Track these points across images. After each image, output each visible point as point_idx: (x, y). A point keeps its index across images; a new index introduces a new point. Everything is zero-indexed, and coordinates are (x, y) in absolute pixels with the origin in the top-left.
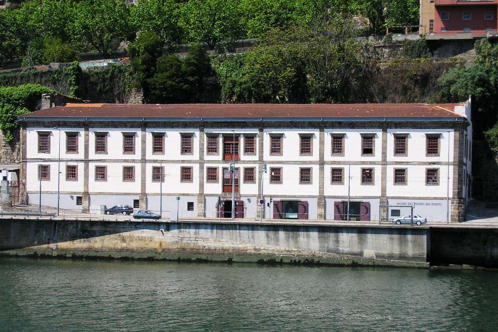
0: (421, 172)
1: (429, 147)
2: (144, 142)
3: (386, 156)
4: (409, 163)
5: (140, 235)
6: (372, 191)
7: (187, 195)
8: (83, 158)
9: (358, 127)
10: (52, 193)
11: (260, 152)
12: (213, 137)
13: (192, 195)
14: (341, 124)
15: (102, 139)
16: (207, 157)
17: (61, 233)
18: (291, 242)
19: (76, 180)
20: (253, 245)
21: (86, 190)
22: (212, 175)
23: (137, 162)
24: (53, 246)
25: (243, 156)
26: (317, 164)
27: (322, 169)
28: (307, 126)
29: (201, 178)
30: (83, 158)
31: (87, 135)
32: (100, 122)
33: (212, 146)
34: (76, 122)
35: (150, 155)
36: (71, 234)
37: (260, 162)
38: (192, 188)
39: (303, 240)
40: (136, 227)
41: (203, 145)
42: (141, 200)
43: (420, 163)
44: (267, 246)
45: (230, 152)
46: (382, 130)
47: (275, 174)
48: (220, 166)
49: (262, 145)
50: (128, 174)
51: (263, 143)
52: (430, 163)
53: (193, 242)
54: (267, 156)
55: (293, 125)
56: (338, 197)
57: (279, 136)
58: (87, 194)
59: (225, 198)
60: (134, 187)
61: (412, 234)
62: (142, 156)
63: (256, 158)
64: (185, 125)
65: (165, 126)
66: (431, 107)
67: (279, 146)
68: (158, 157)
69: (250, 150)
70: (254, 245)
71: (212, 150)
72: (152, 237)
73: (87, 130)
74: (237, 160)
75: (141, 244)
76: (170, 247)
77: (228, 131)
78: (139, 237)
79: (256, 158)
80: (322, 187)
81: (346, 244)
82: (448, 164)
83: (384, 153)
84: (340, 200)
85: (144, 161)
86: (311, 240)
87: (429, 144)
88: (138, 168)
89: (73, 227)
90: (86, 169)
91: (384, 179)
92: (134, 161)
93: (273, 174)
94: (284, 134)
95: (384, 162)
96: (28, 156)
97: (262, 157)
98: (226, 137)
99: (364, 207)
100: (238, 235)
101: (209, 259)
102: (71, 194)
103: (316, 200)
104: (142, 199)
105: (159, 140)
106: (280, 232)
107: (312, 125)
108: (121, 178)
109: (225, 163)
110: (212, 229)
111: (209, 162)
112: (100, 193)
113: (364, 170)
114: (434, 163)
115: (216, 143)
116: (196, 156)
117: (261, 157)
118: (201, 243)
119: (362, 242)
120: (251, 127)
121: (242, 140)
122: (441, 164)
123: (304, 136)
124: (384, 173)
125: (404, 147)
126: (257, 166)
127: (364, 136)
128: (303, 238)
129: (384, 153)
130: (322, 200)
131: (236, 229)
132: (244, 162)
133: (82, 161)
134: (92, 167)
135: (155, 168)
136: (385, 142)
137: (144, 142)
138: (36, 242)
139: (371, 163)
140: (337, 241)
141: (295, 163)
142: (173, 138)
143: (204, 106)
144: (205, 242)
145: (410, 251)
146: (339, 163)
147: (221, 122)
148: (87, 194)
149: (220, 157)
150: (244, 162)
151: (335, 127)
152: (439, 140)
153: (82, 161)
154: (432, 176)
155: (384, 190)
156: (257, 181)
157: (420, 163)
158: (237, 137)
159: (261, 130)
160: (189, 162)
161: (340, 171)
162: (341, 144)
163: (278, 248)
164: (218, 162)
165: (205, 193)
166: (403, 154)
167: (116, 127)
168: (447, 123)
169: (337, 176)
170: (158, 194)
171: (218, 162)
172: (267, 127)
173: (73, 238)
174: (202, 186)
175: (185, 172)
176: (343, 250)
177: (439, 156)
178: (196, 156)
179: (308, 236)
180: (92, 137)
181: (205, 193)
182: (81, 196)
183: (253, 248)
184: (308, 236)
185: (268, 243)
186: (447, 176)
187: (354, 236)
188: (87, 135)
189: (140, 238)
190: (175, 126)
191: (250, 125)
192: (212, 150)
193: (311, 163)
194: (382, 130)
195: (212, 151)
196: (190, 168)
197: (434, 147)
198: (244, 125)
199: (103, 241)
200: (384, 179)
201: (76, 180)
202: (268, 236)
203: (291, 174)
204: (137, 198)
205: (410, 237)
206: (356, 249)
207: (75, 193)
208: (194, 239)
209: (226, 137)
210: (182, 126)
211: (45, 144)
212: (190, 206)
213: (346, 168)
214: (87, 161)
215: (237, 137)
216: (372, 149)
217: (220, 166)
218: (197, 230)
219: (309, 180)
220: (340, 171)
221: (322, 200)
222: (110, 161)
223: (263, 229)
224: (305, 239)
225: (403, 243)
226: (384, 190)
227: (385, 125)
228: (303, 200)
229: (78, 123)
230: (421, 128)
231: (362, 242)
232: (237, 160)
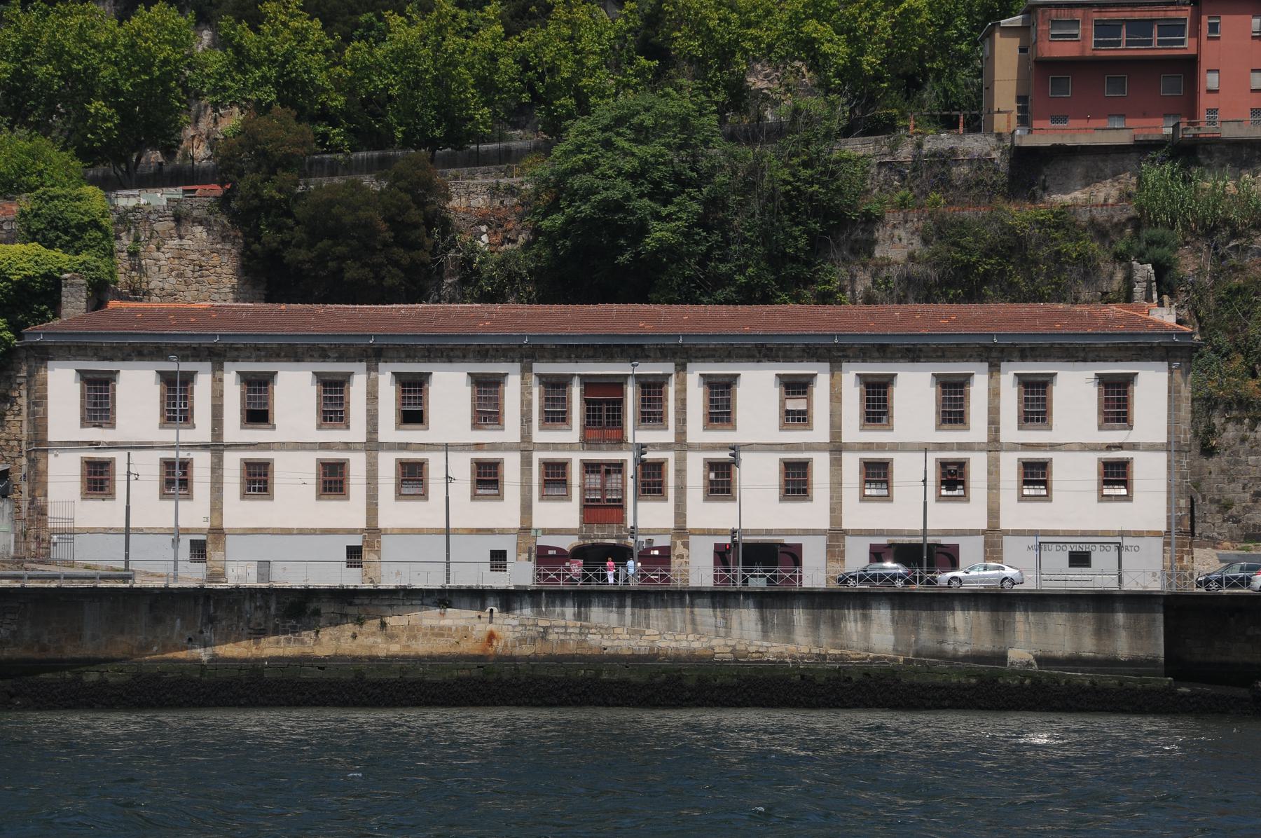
0: (148, 466)
1: (1106, 407)
2: (372, 396)
3: (997, 430)
4: (1058, 447)
5: (434, 623)
7: (490, 531)
8: (207, 438)
9: (925, 357)
10: (106, 531)
11: (677, 420)
12: (555, 387)
13: (503, 532)
14: (884, 351)
15: (260, 391)
16: (539, 436)
17: (224, 623)
18: (825, 631)
19: (499, 496)
20: (730, 643)
21: (216, 524)
22: (555, 475)
23: (355, 450)
25: (636, 434)
26: (824, 450)
27: (836, 464)
28: (798, 357)
29: (526, 486)
30: (207, 438)
31: (218, 382)
32: (257, 348)
33: (553, 406)
34: (189, 347)
35: (1010, 431)
36: (252, 625)
37: (677, 447)
39: (853, 629)
40: (422, 604)
41: (530, 404)
42: (368, 546)
43: (1085, 447)
44: (765, 644)
46: (986, 365)
47: (717, 476)
48: (576, 459)
51: (685, 400)
52: (1110, 447)
53: (573, 637)
54: (696, 431)
55: (762, 352)
56: (880, 533)
57: (727, 380)
58: (218, 532)
59: (589, 538)
61: (1127, 610)
62: (368, 432)
63: (668, 436)
64: (483, 354)
65: (429, 357)
67: (728, 407)
69: (651, 415)
70: (733, 643)
71: (555, 416)
72: (466, 629)
74: (619, 442)
75: (440, 647)
76: (517, 651)
78: (432, 628)
79: (668, 436)
80: (836, 509)
81: (962, 637)
82: (1152, 447)
83: (994, 423)
84: (883, 541)
85: (372, 445)
86: (874, 627)
87: (1107, 399)
88: (357, 464)
89: (256, 608)
90: (217, 468)
91: (993, 486)
92: (347, 446)
93: (712, 476)
94: (739, 375)
95: (994, 445)
96: (53, 436)
97: (685, 433)
98: (590, 384)
99: (944, 556)
100: (688, 617)
101: (101, 656)
102: (177, 533)
103: (822, 541)
104: (370, 545)
105: (879, 393)
106: (796, 611)
107: (812, 353)
108: (775, 493)
109: (590, 449)
110: (622, 606)
111: (546, 446)
112: (256, 529)
113: (168, 465)
115: (565, 401)
116: (511, 431)
117: (681, 433)
118: (594, 639)
119: (999, 629)
120: (656, 360)
121: (576, 392)
122: (1138, 450)
123: (792, 380)
124: (993, 471)
125: (1044, 406)
126: (670, 456)
127: (943, 380)
128: (853, 624)
129: (994, 423)
130: (836, 536)
131: (682, 605)
133: (205, 447)
134: (233, 463)
136: (994, 394)
137: (372, 396)
138: (155, 648)
139: (962, 447)
144: (605, 636)
145: (1123, 646)
146: (881, 447)
147: (578, 346)
148: (218, 532)
149: (573, 434)
151: (870, 357)
152: (1130, 388)
153: (205, 447)
155: (993, 513)
156: (671, 493)
157: (1085, 447)
158: (617, 384)
159: (681, 368)
160: (494, 447)
161: (1044, 466)
162: (885, 400)
163: (792, 647)
164: (569, 447)
166: (959, 426)
167: (298, 360)
168: (1152, 348)
170: (437, 532)
172: (696, 357)
173: (258, 633)
174: (526, 508)
175: (723, 473)
176: (955, 649)
177: (1131, 428)
178: (511, 431)
180: (1008, 379)
181: (689, 525)
182: (203, 538)
183: (729, 649)
184: (866, 618)
185: (765, 634)
187: (982, 618)
188: (218, 382)
189: (436, 630)
190: (458, 357)
191: (652, 354)
192: (555, 416)
193: (810, 447)
194: (986, 365)
195: (553, 420)
196: (498, 463)
197: (879, 407)
198: (634, 351)
199: (338, 639)
200: (993, 486)
201: (499, 496)
202: (763, 620)
204: (356, 541)
206: (986, 644)
207: (187, 531)
208: (577, 631)
209: (590, 384)
210: (474, 357)
211: (101, 404)
212: (498, 558)
213: (120, 457)
214: (217, 447)
215: (617, 384)
216: (267, 411)
217: (576, 459)
218: (836, 611)
219: (805, 491)
220: (1044, 466)
221: (836, 536)
222: (283, 446)
223: (751, 602)
224: (859, 624)
225: (1103, 630)
226: (993, 513)
227: (994, 354)
228: (788, 540)
229: (194, 348)
230: (1085, 360)
231: (999, 629)
232: (619, 442)
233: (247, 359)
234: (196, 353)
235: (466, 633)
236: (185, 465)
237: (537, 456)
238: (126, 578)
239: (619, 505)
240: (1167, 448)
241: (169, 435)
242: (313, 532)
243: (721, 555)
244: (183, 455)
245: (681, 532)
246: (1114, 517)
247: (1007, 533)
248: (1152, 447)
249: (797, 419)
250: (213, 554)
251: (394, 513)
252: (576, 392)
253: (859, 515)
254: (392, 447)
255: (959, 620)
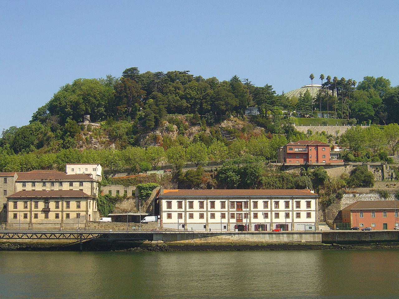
0: (22, 214)
6: (289, 220)
10: (219, 223)
13: (225, 223)
16: (230, 210)
24: (182, 242)
25: (243, 210)
27: (271, 213)
31: (185, 203)
38: (225, 221)
45: (239, 207)
48: (235, 213)
49: (250, 205)
50: (202, 216)
54: (252, 209)
56: (278, 223)
60: (204, 221)
63: (248, 210)
64: (223, 199)
66: (200, 192)
68: (68, 210)
69: (246, 207)
73: (63, 201)
77: (245, 200)
80: (271, 219)
82: (313, 211)
91: (293, 216)
92: (204, 211)
95: (293, 211)
111: (231, 211)
113: (179, 214)
114: (309, 211)
116: (226, 209)
117: (250, 209)
119: (301, 237)
124: (293, 214)
132: (244, 211)
133: (184, 212)
135: (276, 213)
139: (288, 211)
140: (293, 238)
141: (176, 211)
142: (218, 203)
143: (240, 190)
146: (278, 211)
149: (235, 210)
150: (244, 211)
153: (184, 212)
154: (309, 215)
155: (293, 220)
160: (224, 211)
164: (235, 211)
165: (208, 222)
169: (277, 216)
171: (235, 211)
174: (229, 220)
178: (226, 209)
179: (283, 236)
184: (283, 236)
186: (313, 214)
200: (293, 216)
203: (282, 215)
205: (316, 235)
207: (182, 223)
213: (18, 213)
215: (241, 202)
221: (271, 224)
225: (314, 237)
226: (293, 220)
233: (190, 199)
234: (183, 199)
235: (229, 239)
236: (181, 214)
237: (230, 212)
238: (356, 229)
239: (242, 220)
240: (163, 212)
241: (78, 210)
242: (215, 223)
243: (277, 226)
244: (80, 212)
245: (250, 223)
246: (309, 220)
247: (188, 223)
248: (313, 211)
249: (26, 207)
250: (185, 227)
251: (210, 221)
252: (235, 203)
253: (275, 220)
254: (210, 211)
255: (295, 236)
